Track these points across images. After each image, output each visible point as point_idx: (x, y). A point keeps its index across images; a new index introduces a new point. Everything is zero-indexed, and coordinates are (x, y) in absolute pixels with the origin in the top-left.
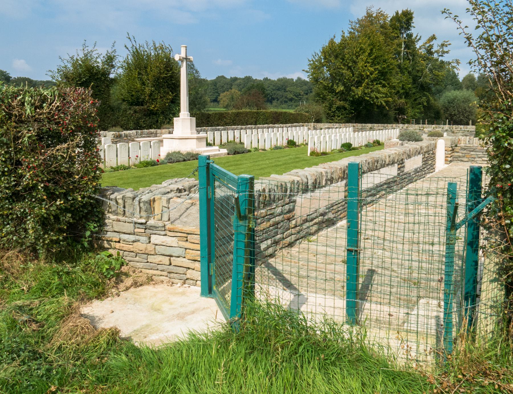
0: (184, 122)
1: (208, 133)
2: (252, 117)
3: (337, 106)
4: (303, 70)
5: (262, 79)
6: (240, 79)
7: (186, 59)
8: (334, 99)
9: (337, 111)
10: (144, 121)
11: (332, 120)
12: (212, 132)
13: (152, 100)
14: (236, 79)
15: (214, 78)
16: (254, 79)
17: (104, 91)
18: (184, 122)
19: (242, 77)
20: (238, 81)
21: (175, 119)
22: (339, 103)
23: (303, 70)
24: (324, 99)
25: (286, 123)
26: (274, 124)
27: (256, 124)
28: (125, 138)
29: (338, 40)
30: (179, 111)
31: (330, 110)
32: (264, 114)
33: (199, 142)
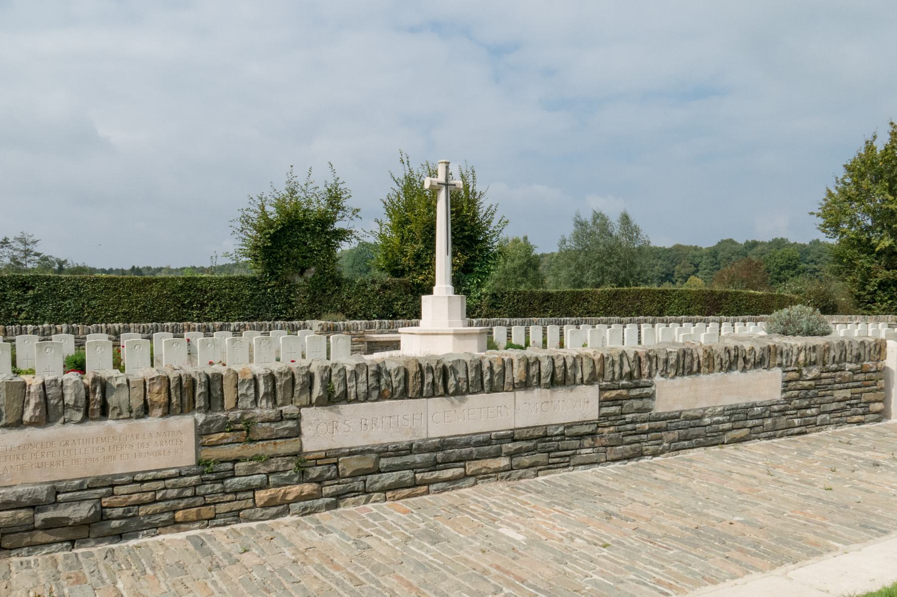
0: (441, 307)
1: (684, 324)
2: (652, 301)
3: (878, 280)
4: (812, 214)
5: (807, 243)
6: (763, 243)
7: (447, 185)
8: (872, 266)
9: (879, 292)
10: (403, 305)
11: (869, 309)
12: (558, 327)
13: (422, 267)
14: (755, 244)
15: (712, 243)
16: (792, 242)
17: (319, 251)
18: (441, 307)
19: (767, 239)
20: (759, 248)
21: (424, 297)
22: (883, 274)
23: (812, 214)
24: (851, 264)
25: (739, 312)
26: (707, 315)
27: (661, 313)
29: (880, 146)
30: (433, 284)
31: (864, 290)
32: (681, 295)
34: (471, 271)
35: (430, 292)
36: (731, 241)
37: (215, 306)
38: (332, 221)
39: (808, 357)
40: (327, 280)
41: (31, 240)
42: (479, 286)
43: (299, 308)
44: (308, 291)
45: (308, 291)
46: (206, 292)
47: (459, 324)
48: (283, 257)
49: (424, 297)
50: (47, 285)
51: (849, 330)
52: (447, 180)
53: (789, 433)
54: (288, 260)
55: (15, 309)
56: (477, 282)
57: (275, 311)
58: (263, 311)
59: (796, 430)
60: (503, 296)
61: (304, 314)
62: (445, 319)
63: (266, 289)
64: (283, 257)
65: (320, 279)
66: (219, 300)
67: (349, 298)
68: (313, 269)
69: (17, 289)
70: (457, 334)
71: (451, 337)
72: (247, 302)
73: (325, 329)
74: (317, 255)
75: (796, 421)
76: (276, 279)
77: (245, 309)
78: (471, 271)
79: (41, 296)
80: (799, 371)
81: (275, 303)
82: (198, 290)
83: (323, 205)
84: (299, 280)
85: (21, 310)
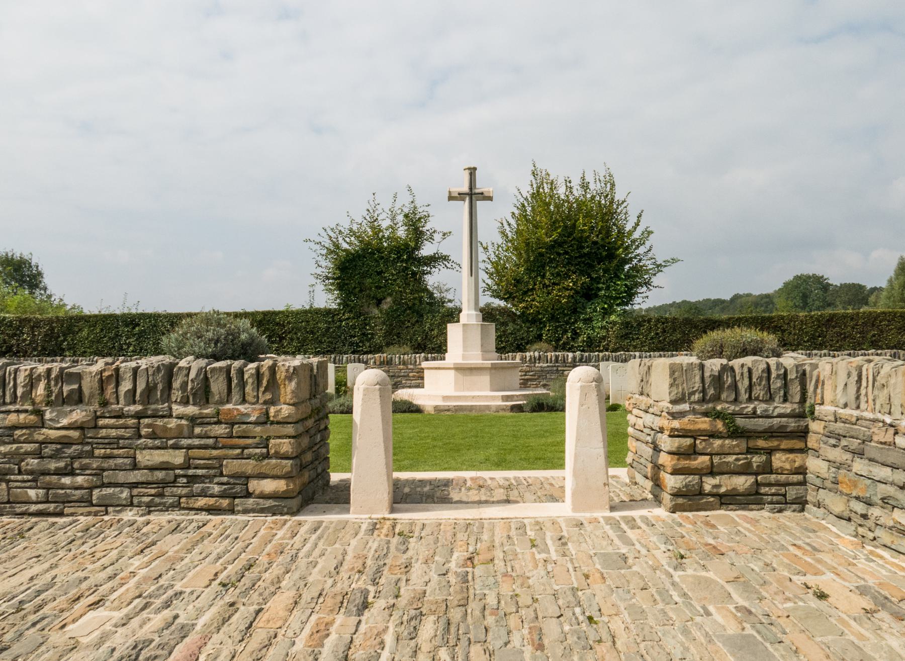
17: (395, 280)
28: (402, 367)
33: (460, 376)
34: (596, 296)
37: (292, 339)
38: (417, 248)
39: (55, 390)
40: (406, 310)
41: (445, 288)
42: (606, 313)
43: (378, 340)
44: (383, 323)
45: (383, 323)
46: (284, 326)
48: (355, 288)
49: (450, 326)
50: (150, 321)
51: (790, 359)
52: (471, 189)
53: (18, 510)
54: (361, 291)
55: (125, 344)
56: (603, 308)
57: (351, 344)
58: (340, 344)
59: (33, 508)
60: (640, 325)
61: (381, 347)
62: (478, 352)
63: (341, 321)
64: (355, 288)
65: (397, 310)
66: (296, 333)
67: (433, 330)
68: (389, 299)
69: (127, 326)
70: (494, 367)
71: (453, 372)
72: (324, 335)
73: (378, 363)
74: (392, 284)
75: (32, 493)
76: (350, 311)
77: (321, 342)
78: (596, 296)
79: (144, 331)
80: (39, 413)
81: (351, 336)
82: (278, 324)
83: (402, 233)
84: (376, 312)
85: (129, 345)
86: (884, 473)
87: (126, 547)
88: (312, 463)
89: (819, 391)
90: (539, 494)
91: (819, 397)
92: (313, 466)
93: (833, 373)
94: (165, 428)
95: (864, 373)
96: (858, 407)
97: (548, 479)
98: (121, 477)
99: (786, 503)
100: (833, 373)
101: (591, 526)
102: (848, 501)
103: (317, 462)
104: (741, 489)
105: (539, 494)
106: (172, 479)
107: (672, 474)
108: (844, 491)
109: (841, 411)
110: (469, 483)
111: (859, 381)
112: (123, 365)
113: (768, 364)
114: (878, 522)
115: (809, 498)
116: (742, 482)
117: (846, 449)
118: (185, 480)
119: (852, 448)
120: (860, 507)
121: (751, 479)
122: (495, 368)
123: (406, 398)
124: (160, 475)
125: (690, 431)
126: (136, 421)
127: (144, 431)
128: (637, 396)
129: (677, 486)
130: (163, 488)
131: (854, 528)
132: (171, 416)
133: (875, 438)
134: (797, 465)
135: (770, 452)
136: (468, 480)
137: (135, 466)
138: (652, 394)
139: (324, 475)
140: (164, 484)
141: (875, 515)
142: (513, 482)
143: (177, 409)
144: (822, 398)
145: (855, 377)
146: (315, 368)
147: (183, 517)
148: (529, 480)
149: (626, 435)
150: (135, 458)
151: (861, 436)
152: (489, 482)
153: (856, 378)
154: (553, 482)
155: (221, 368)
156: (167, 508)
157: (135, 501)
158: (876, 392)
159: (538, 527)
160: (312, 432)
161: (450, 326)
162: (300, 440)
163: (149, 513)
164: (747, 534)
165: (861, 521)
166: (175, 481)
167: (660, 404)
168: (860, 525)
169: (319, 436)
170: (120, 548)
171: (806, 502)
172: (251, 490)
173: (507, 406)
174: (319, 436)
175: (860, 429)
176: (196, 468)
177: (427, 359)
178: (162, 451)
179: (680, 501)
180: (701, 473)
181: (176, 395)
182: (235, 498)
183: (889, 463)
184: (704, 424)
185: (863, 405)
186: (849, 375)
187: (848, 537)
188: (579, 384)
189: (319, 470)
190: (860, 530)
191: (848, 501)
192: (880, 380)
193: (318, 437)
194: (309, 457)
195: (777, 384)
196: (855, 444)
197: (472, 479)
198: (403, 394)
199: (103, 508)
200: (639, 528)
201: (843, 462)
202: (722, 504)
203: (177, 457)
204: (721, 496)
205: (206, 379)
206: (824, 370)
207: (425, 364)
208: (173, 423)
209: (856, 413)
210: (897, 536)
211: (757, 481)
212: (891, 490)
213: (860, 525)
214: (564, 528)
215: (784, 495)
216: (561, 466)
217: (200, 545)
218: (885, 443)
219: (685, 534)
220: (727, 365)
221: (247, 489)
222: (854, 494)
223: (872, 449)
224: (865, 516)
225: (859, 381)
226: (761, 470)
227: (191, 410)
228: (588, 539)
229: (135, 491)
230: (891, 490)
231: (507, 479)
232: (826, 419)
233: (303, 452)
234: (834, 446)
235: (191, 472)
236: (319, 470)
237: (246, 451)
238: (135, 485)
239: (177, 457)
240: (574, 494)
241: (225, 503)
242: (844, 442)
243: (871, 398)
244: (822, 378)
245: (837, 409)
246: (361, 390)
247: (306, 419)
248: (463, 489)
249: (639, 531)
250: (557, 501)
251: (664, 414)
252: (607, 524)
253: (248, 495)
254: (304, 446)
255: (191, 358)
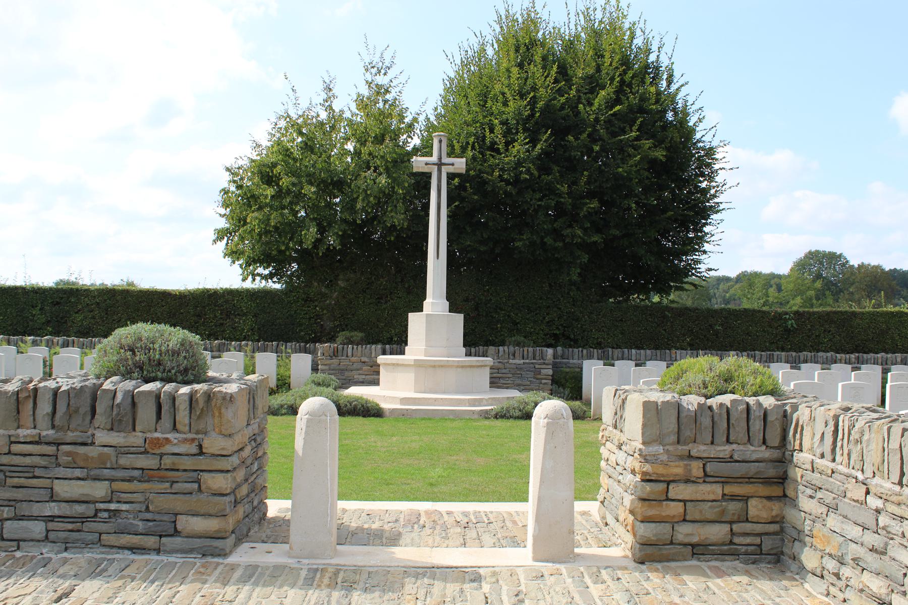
35: (420, 309)
36: (833, 258)
47: (459, 355)
49: (412, 316)
86: (855, 532)
87: (42, 592)
88: (248, 496)
89: (798, 436)
90: (499, 536)
91: (797, 442)
92: (249, 499)
93: (812, 419)
94: (86, 458)
95: (841, 424)
96: (834, 460)
97: (510, 514)
98: (36, 509)
99: (761, 554)
100: (812, 419)
101: (552, 579)
102: (822, 557)
103: (253, 495)
104: (713, 538)
105: (499, 536)
106: (92, 513)
107: (642, 522)
108: (818, 546)
109: (818, 461)
110: (423, 519)
111: (836, 431)
112: (42, 385)
113: (748, 404)
114: (849, 583)
115: (785, 550)
116: (717, 532)
117: (821, 501)
118: (106, 515)
119: (827, 501)
120: (831, 565)
121: (726, 528)
122: (462, 367)
123: (357, 399)
124: (79, 509)
125: (663, 475)
126: (55, 448)
127: (63, 459)
128: (611, 428)
129: (646, 534)
130: (83, 522)
131: (825, 587)
132: (93, 444)
133: (849, 495)
134: (774, 513)
135: (745, 499)
136: (423, 514)
137: (53, 498)
138: (625, 429)
139: (262, 508)
140: (83, 519)
141: (846, 575)
142: (472, 517)
143: (102, 437)
144: (801, 444)
145: (831, 427)
146: (253, 580)
147: (103, 556)
148: (490, 515)
149: (599, 469)
150: (52, 489)
151: (835, 491)
152: (446, 517)
153: (833, 429)
154: (516, 519)
155: (149, 393)
156: (87, 545)
157: (52, 536)
158: (851, 446)
159: (494, 580)
160: (249, 462)
161: (412, 316)
162: (235, 474)
163: (66, 549)
164: (716, 591)
165: (833, 579)
166: (95, 516)
167: (633, 443)
168: (832, 584)
169: (256, 465)
170: (34, 594)
171: (782, 553)
172: (179, 528)
173: (473, 412)
174: (256, 465)
175: (835, 482)
176: (119, 502)
177: (384, 353)
178: (82, 482)
179: (649, 550)
180: (673, 522)
181: (100, 419)
182: (161, 536)
183: (859, 522)
184: (677, 469)
185: (838, 458)
186: (826, 424)
187: (819, 596)
188: (546, 421)
189: (255, 503)
190: (832, 589)
191: (822, 557)
192: (855, 435)
193: (256, 466)
194: (244, 490)
195: (757, 425)
196: (829, 498)
197: (427, 513)
198: (355, 391)
199: (15, 543)
200: (603, 582)
201: (819, 515)
202: (694, 554)
203: (99, 490)
204: (693, 546)
205: (134, 404)
206: (803, 414)
207: (382, 359)
208: (92, 452)
209: (832, 465)
210: (866, 600)
211: (731, 530)
212: (861, 552)
213: (832, 584)
214: (522, 581)
215: (760, 546)
216: (526, 500)
217: (122, 593)
218: (857, 501)
219: (651, 591)
220: (705, 404)
221: (175, 528)
222: (827, 551)
223: (845, 506)
224: (837, 576)
225: (836, 431)
226: (735, 518)
227: (116, 438)
228: (547, 596)
229: (51, 525)
230: (861, 552)
231: (466, 514)
232: (803, 467)
233: (239, 486)
234: (811, 497)
235: (113, 506)
236: (255, 503)
237: (175, 485)
238: (52, 518)
239: (99, 490)
240: (535, 538)
241: (151, 541)
242: (819, 495)
243: (846, 452)
244: (801, 423)
245: (814, 458)
246: (304, 421)
247: (241, 449)
248: (416, 526)
249: (603, 586)
250: (518, 545)
251: (636, 455)
252: (569, 577)
253: (176, 533)
254: (239, 480)
255: (115, 379)
